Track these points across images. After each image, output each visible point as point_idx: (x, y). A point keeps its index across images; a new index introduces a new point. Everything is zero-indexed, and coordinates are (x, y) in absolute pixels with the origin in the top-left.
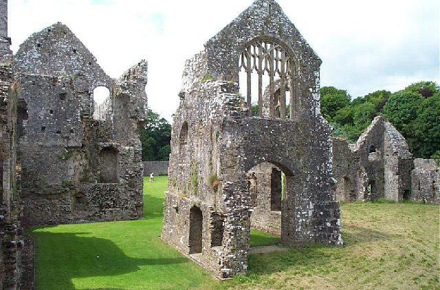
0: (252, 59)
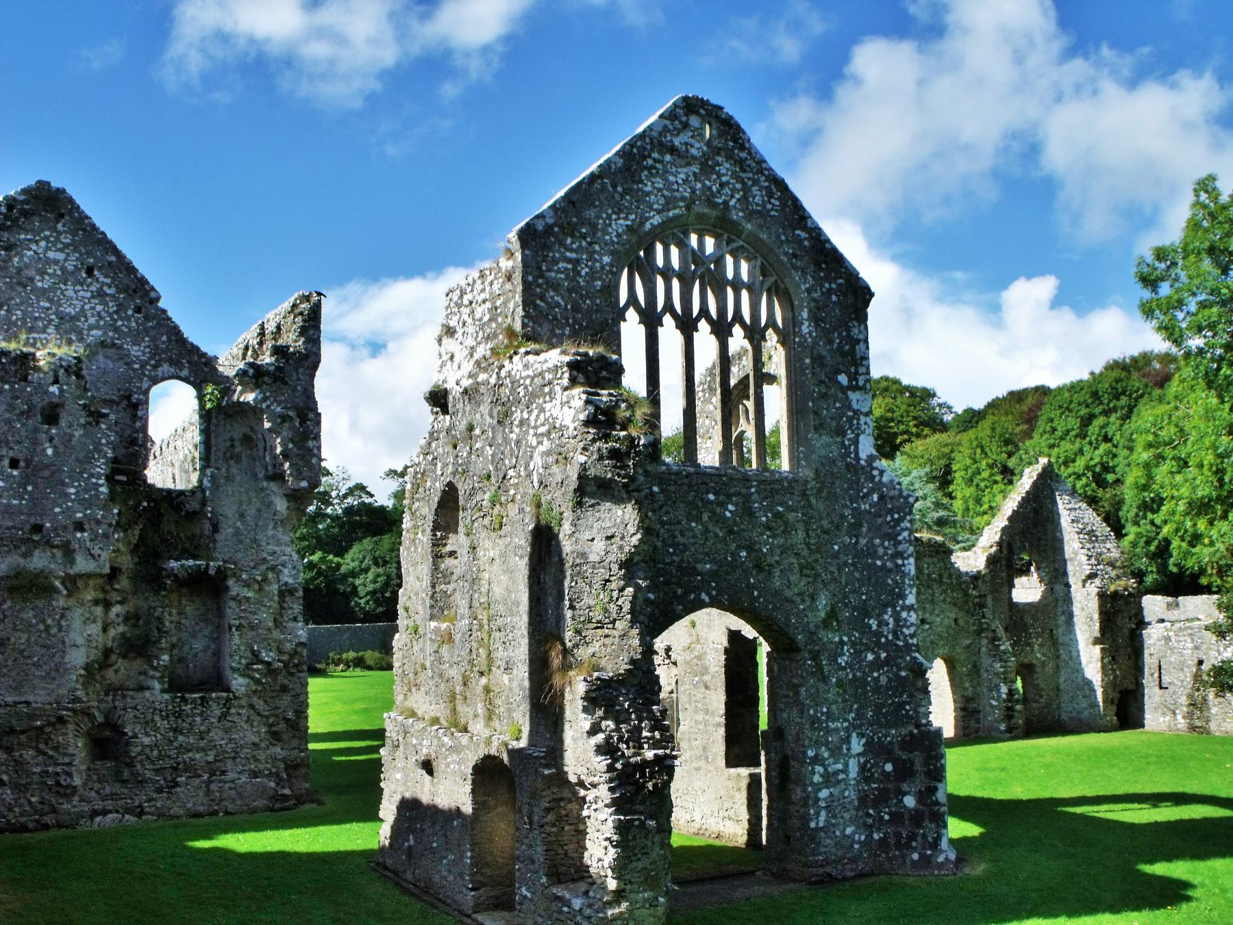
0: (660, 282)
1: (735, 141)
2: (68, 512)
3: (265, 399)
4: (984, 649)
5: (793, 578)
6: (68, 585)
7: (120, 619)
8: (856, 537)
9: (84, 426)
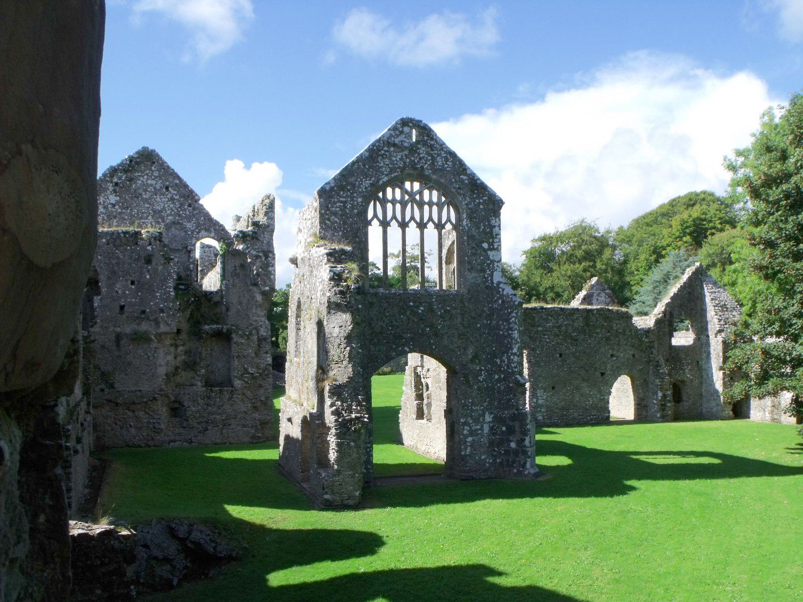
1: (428, 136)
2: (157, 304)
3: (247, 248)
4: (651, 372)
5: (454, 340)
6: (158, 337)
7: (183, 353)
8: (491, 320)
9: (163, 264)
